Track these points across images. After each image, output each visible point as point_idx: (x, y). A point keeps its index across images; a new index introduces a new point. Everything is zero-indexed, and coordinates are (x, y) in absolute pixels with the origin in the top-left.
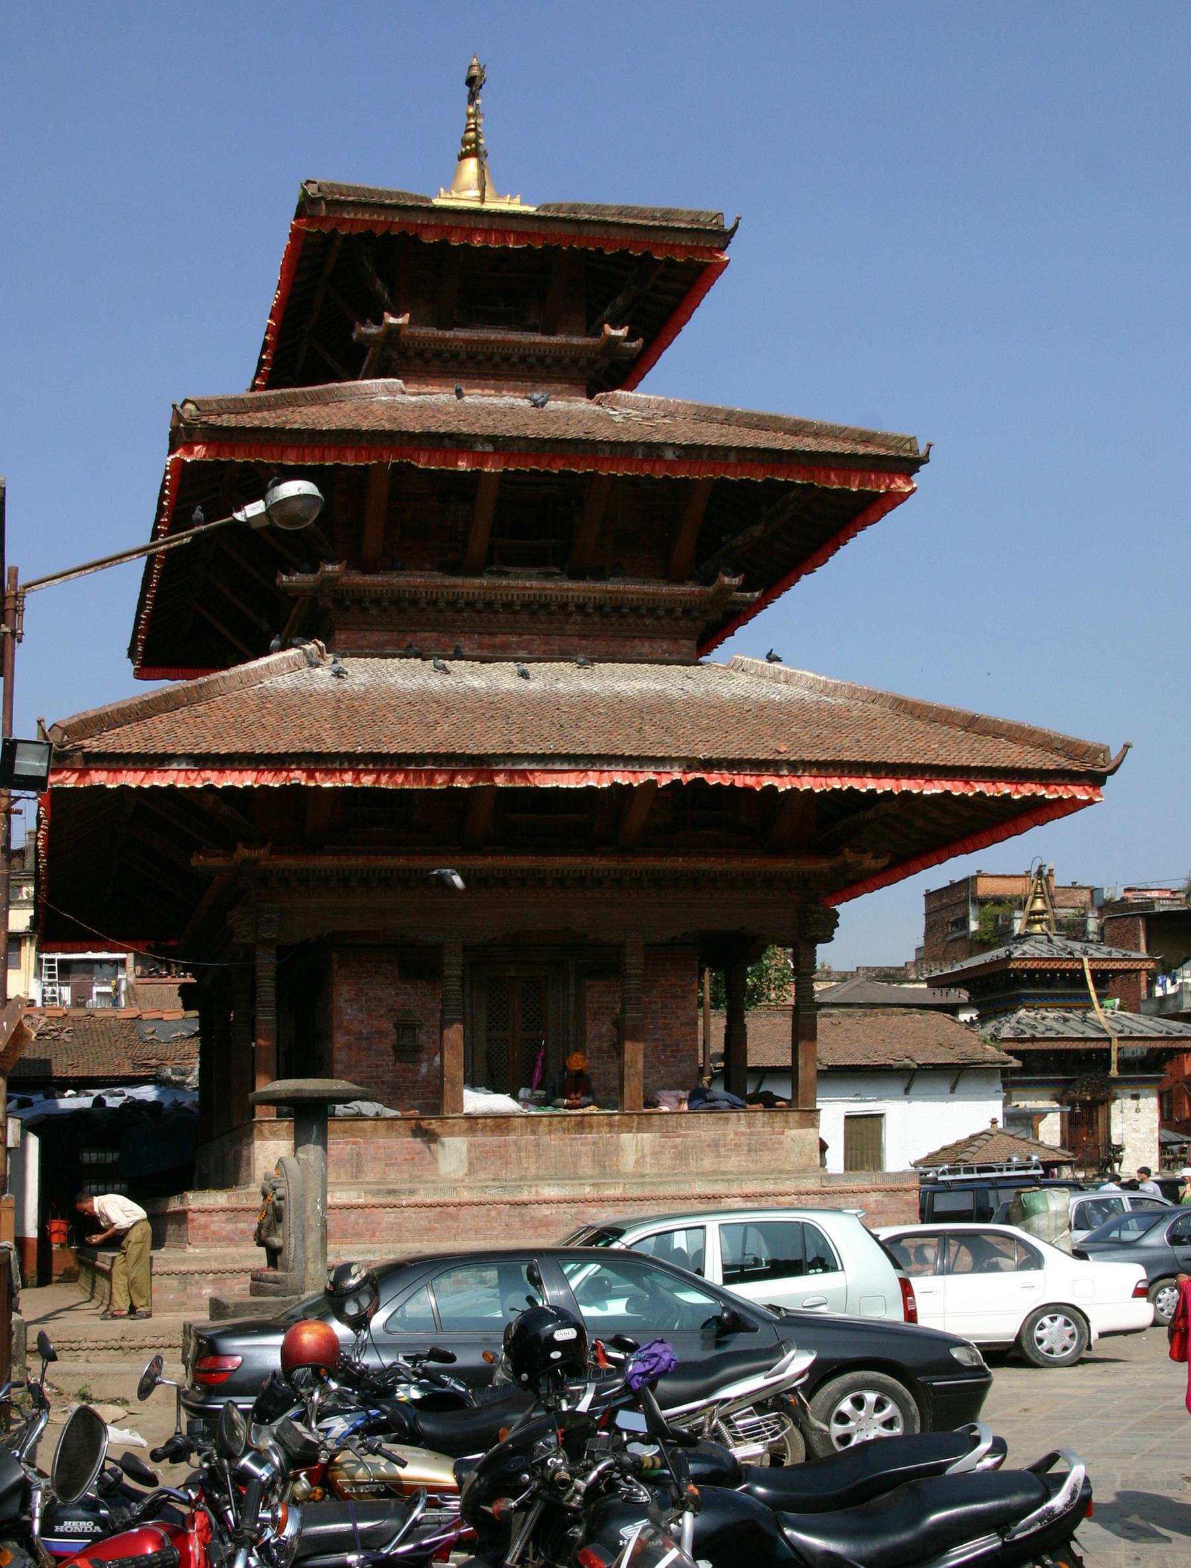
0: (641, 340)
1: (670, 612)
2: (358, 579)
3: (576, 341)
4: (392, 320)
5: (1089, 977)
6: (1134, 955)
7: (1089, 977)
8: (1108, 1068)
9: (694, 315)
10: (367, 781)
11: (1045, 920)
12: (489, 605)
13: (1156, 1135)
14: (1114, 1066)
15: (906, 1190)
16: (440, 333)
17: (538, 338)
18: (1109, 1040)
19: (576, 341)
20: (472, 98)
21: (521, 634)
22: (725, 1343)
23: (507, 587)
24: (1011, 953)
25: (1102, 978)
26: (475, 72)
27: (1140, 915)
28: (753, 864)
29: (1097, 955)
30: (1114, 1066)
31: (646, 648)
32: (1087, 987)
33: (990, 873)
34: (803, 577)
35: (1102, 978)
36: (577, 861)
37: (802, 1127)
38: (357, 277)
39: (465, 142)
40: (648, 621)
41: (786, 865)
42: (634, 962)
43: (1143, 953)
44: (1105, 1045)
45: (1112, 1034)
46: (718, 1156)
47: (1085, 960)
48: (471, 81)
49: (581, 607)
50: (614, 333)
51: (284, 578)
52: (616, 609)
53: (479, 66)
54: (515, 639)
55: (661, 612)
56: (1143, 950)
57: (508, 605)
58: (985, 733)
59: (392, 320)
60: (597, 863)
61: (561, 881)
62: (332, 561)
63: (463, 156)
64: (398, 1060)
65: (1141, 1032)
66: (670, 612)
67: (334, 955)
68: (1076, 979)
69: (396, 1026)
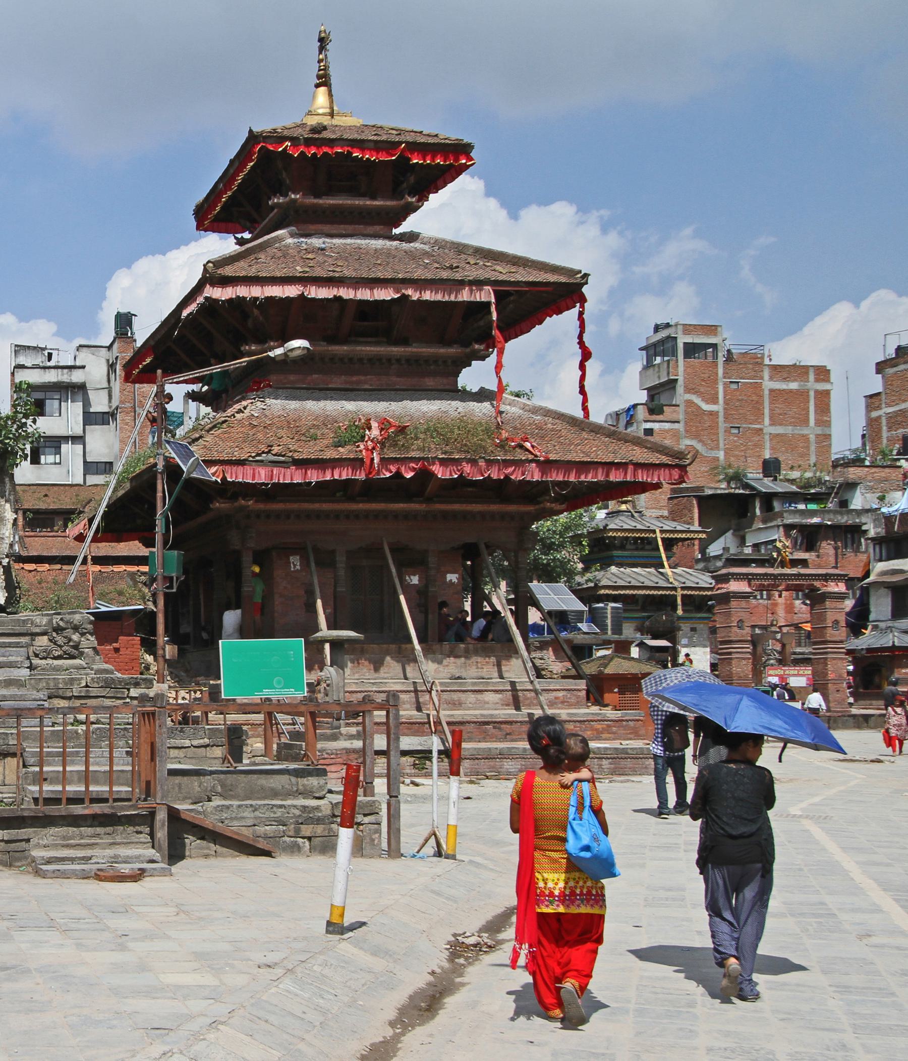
1: (445, 362)
3: (389, 203)
4: (293, 196)
5: (660, 543)
6: (692, 528)
7: (660, 543)
8: (675, 608)
9: (533, 330)
11: (629, 501)
12: (351, 360)
13: (709, 657)
14: (680, 607)
15: (579, 690)
16: (316, 201)
18: (675, 589)
19: (389, 203)
20: (322, 49)
22: (140, 869)
24: (607, 525)
25: (669, 544)
26: (323, 35)
27: (694, 496)
28: (494, 507)
29: (666, 528)
30: (680, 607)
31: (429, 382)
32: (658, 549)
33: (784, 754)
35: (669, 544)
36: (405, 505)
39: (319, 77)
41: (512, 508)
43: (696, 527)
44: (673, 593)
45: (676, 584)
46: (477, 668)
47: (658, 531)
48: (321, 40)
49: (398, 361)
50: (410, 200)
52: (417, 361)
53: (325, 31)
54: (362, 378)
56: (696, 523)
57: (361, 360)
58: (619, 440)
59: (293, 196)
60: (414, 506)
61: (396, 516)
63: (317, 86)
65: (697, 583)
66: (445, 362)
68: (651, 544)
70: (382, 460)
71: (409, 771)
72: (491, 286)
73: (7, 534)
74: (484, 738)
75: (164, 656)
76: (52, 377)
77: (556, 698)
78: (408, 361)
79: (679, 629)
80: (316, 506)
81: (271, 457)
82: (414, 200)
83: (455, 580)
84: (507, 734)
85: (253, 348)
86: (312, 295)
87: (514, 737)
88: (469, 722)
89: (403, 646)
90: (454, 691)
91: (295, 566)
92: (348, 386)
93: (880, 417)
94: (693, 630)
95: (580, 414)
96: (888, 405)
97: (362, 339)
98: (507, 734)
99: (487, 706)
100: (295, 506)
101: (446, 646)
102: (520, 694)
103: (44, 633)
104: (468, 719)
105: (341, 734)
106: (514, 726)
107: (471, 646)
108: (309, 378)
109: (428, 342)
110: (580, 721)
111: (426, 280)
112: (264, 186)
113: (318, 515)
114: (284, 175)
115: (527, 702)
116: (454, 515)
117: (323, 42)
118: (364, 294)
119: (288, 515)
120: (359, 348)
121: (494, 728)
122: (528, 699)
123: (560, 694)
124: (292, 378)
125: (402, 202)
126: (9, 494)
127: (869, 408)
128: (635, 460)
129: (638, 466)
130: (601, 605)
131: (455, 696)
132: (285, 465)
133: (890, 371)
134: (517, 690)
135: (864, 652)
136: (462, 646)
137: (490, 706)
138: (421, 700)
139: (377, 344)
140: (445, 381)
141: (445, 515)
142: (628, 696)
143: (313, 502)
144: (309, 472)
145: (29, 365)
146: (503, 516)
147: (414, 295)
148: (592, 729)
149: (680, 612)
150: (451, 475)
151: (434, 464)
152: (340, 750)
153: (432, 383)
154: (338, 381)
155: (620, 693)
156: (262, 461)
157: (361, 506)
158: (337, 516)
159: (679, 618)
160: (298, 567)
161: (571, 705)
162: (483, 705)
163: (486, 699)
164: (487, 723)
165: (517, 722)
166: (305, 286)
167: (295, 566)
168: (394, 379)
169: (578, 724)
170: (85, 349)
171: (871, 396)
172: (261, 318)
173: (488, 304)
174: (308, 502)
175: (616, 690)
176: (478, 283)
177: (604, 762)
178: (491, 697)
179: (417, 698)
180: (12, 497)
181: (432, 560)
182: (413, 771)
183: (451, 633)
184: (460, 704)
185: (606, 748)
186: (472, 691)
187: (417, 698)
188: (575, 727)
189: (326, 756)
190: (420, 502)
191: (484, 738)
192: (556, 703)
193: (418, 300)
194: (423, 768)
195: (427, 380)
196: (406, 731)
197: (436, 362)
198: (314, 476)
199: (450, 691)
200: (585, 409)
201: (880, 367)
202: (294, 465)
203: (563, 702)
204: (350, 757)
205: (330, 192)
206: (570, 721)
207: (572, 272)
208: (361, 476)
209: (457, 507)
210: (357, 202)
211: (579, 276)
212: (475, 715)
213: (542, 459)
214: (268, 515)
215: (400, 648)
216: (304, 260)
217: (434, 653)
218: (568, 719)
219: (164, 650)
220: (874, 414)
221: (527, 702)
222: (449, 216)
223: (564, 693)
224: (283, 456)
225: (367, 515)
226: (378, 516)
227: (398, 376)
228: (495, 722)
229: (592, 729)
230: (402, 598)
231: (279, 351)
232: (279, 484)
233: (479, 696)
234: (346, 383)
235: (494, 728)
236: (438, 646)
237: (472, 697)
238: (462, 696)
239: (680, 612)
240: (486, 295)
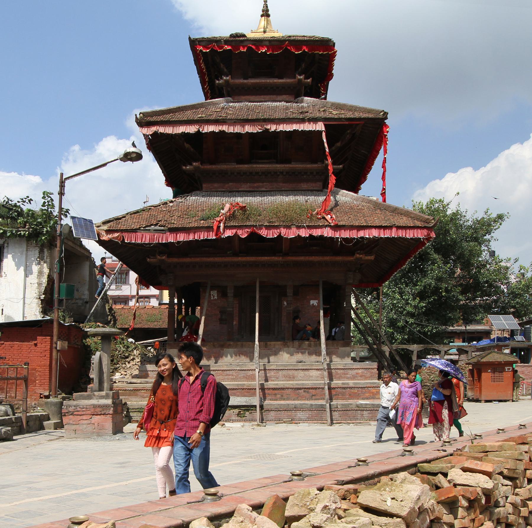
0: (311, 79)
2: (208, 167)
4: (299, 77)
10: (191, 238)
12: (251, 173)
16: (245, 81)
17: (276, 80)
21: (263, 183)
23: (257, 167)
31: (304, 186)
34: (170, 188)
37: (344, 347)
38: (226, 63)
40: (305, 177)
42: (290, 292)
49: (282, 173)
51: (184, 167)
54: (261, 184)
55: (309, 174)
57: (257, 173)
60: (275, 259)
62: (195, 161)
64: (220, 323)
67: (201, 290)
69: (220, 312)
70: (224, 226)
71: (234, 418)
72: (323, 121)
73: (44, 281)
74: (297, 398)
75: (56, 348)
77: (357, 374)
78: (287, 173)
80: (211, 259)
81: (157, 228)
82: (302, 77)
84: (313, 396)
85: (188, 167)
86: (205, 131)
87: (317, 397)
88: (288, 388)
89: (269, 343)
90: (290, 370)
91: (214, 297)
92: (251, 189)
95: (381, 199)
97: (260, 161)
98: (313, 396)
99: (311, 378)
100: (198, 260)
101: (296, 343)
102: (333, 371)
104: (288, 386)
105: (94, 395)
106: (318, 391)
107: (312, 343)
108: (227, 185)
110: (361, 388)
111: (279, 119)
114: (222, 65)
115: (338, 376)
118: (238, 129)
120: (255, 166)
121: (304, 391)
122: (338, 374)
123: (360, 371)
124: (216, 185)
125: (296, 80)
126: (47, 258)
128: (397, 224)
129: (399, 228)
130: (528, 326)
131: (291, 373)
132: (163, 232)
134: (331, 369)
136: (307, 343)
137: (313, 378)
138: (268, 375)
140: (314, 185)
142: (497, 374)
143: (209, 257)
144: (178, 236)
147: (273, 128)
148: (370, 392)
150: (273, 235)
151: (261, 229)
152: (89, 405)
153: (305, 186)
154: (245, 187)
155: (492, 372)
156: (149, 230)
160: (216, 297)
161: (366, 378)
162: (309, 378)
163: (311, 374)
164: (300, 389)
165: (319, 388)
166: (200, 126)
167: (214, 297)
168: (281, 184)
169: (360, 389)
172: (192, 149)
173: (320, 132)
174: (206, 257)
175: (489, 371)
176: (315, 120)
177: (365, 412)
178: (314, 373)
179: (266, 374)
180: (48, 260)
182: (237, 418)
183: (299, 336)
184: (294, 377)
185: (367, 404)
186: (301, 369)
187: (266, 374)
188: (358, 391)
189: (79, 409)
191: (297, 398)
192: (356, 377)
193: (275, 131)
194: (244, 416)
195: (302, 184)
196: (246, 394)
198: (182, 237)
199: (287, 370)
200: (383, 194)
202: (170, 232)
203: (361, 376)
204: (96, 410)
206: (355, 388)
208: (212, 236)
209: (302, 258)
210: (268, 81)
211: (382, 114)
212: (292, 384)
213: (332, 224)
215: (266, 344)
217: (288, 347)
218: (354, 386)
219: (57, 344)
221: (338, 376)
223: (363, 370)
224: (164, 226)
226: (255, 265)
228: (305, 388)
229: (370, 392)
230: (257, 315)
232: (159, 243)
233: (306, 373)
234: (250, 187)
235: (304, 391)
236: (291, 343)
237: (301, 373)
238: (296, 373)
240: (320, 127)
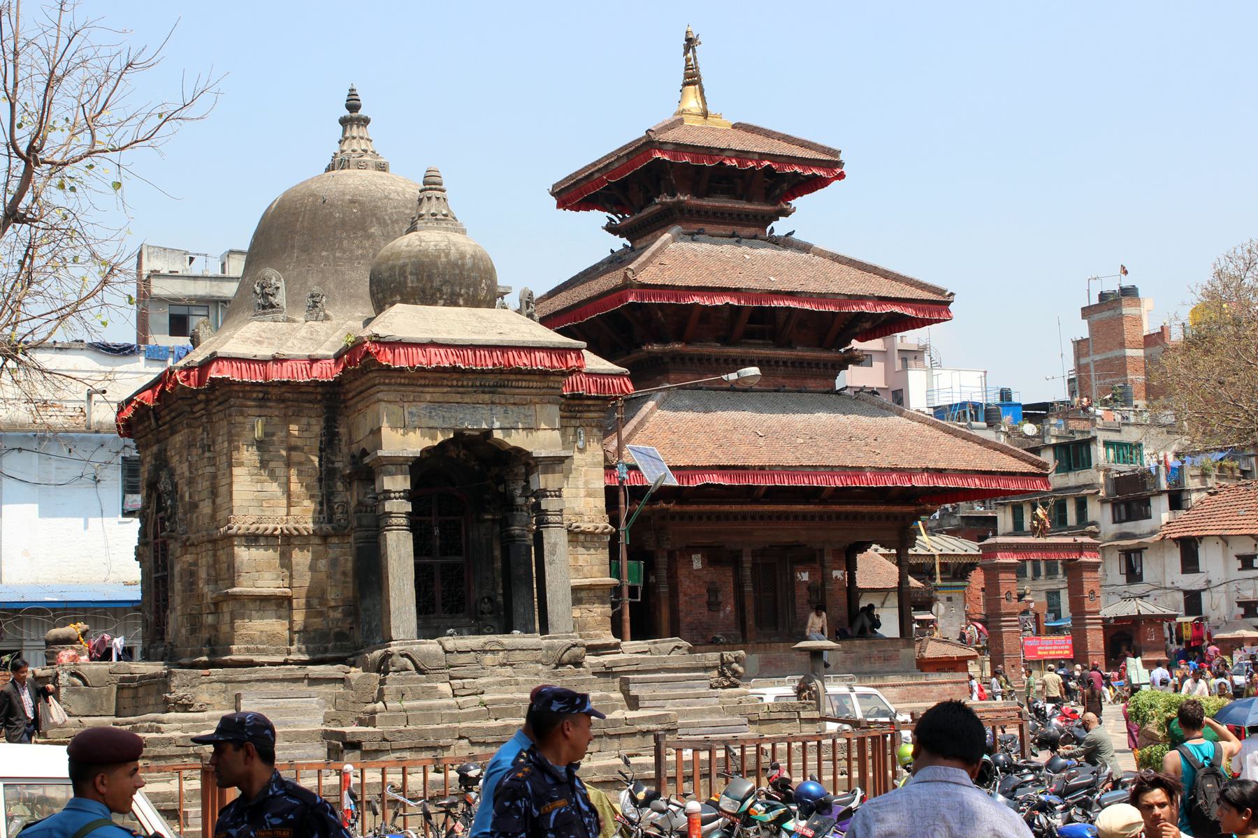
14: (938, 576)
18: (933, 556)
30: (938, 576)
41: (896, 509)
49: (785, 363)
60: (811, 508)
61: (796, 516)
76: (201, 289)
78: (793, 363)
79: (937, 600)
80: (727, 508)
83: (840, 576)
93: (1088, 364)
94: (949, 599)
96: (1096, 352)
100: (707, 508)
103: (714, 667)
109: (809, 345)
112: (640, 186)
113: (728, 516)
116: (847, 516)
117: (690, 43)
119: (700, 516)
123: (948, 686)
127: (1078, 355)
133: (1097, 317)
135: (1112, 621)
137: (530, 656)
139: (765, 346)
141: (839, 516)
143: (721, 503)
145: (165, 271)
146: (888, 516)
149: (938, 582)
157: (766, 508)
158: (744, 516)
159: (936, 588)
170: (236, 256)
171: (1078, 342)
181: (828, 558)
190: (815, 504)
197: (817, 365)
201: (1087, 312)
205: (707, 194)
207: (941, 292)
209: (849, 508)
214: (682, 516)
216: (686, 262)
220: (1083, 361)
222: (806, 217)
225: (770, 516)
227: (784, 378)
231: (733, 376)
239: (938, 582)
